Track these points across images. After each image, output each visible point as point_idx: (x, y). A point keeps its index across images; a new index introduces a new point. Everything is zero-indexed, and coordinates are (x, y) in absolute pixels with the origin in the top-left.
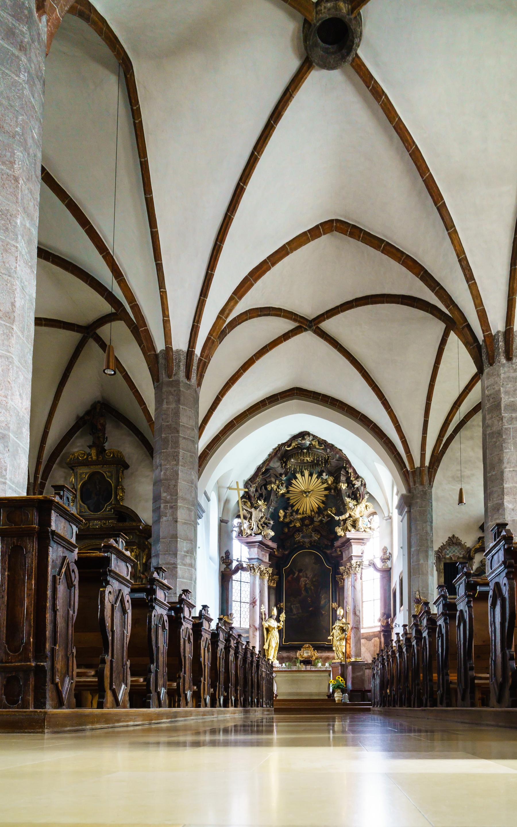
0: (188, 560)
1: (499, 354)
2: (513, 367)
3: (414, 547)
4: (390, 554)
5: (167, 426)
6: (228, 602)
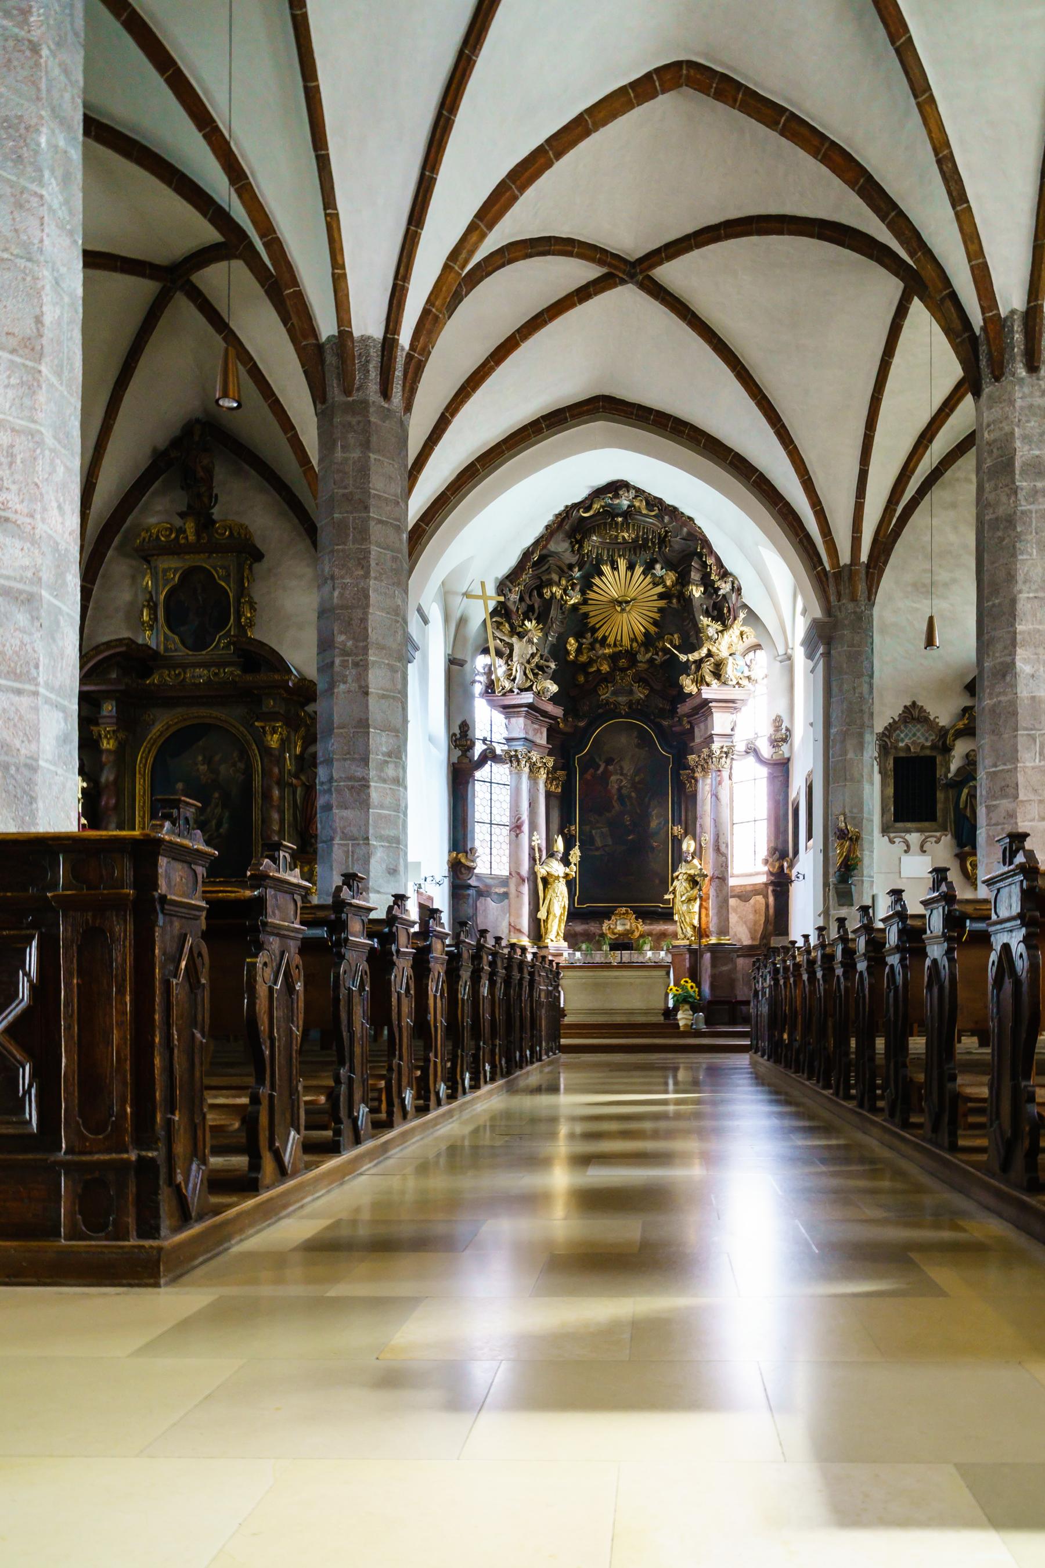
0: (390, 771)
1: (1013, 358)
2: (1040, 386)
3: (835, 726)
4: (787, 730)
5: (344, 495)
6: (467, 826)
